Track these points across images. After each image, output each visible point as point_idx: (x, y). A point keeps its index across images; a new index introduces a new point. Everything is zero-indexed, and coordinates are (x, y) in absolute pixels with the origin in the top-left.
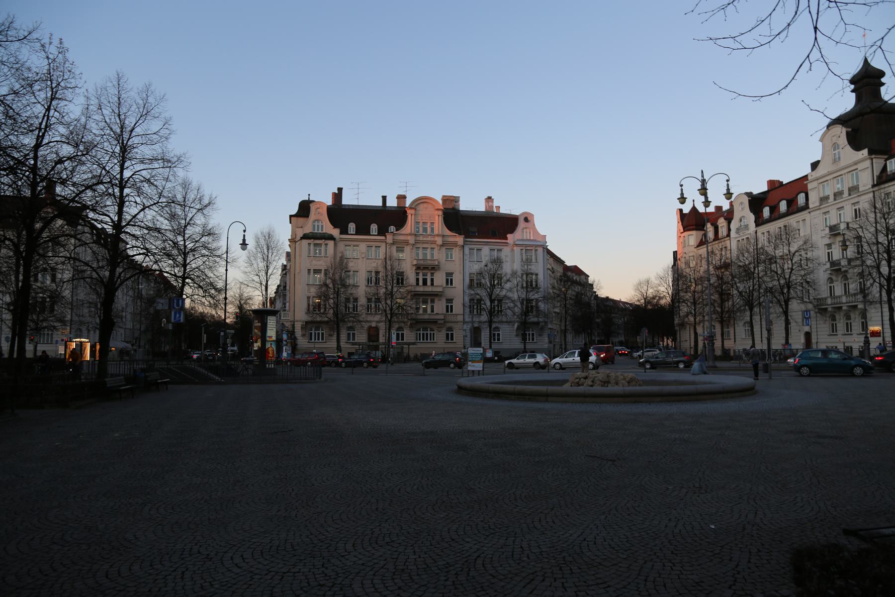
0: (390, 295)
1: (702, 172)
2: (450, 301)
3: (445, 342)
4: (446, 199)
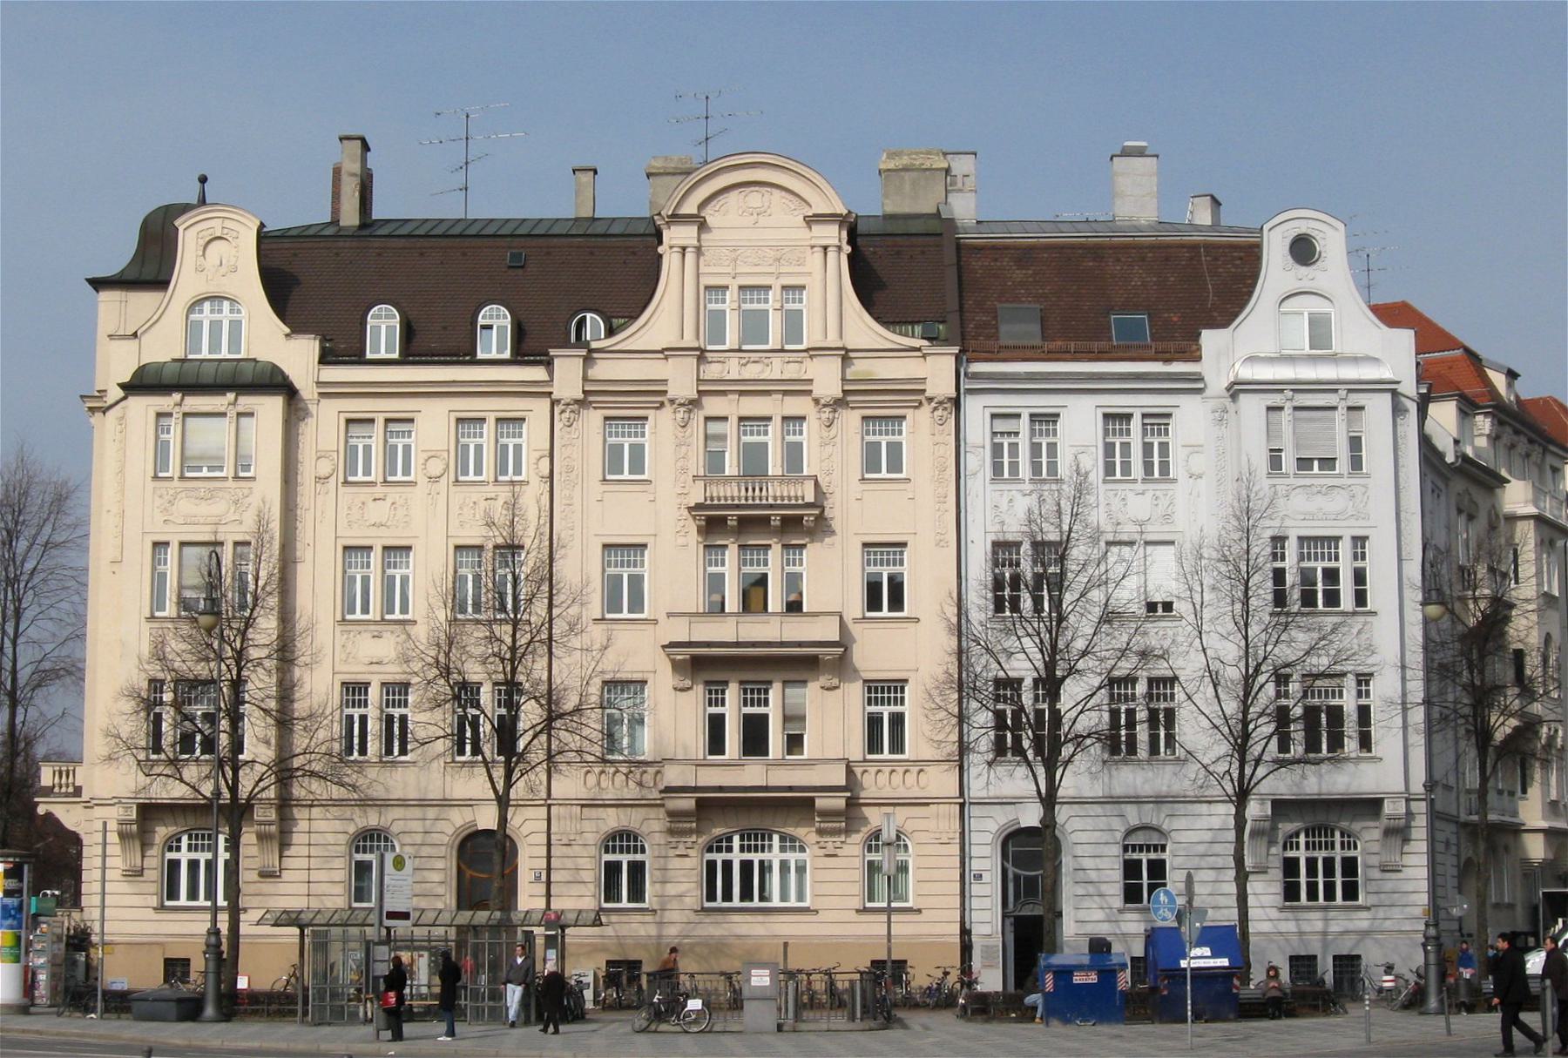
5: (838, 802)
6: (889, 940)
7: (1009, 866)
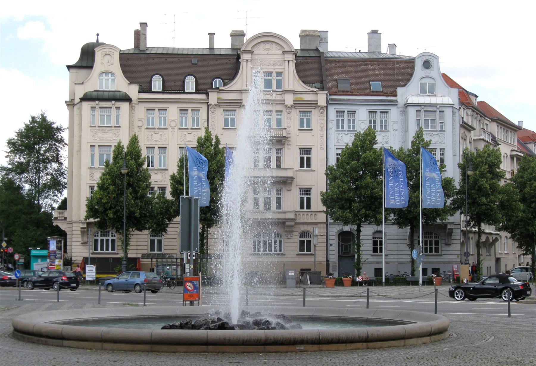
2: (306, 191)
4: (305, 36)
5: (292, 223)
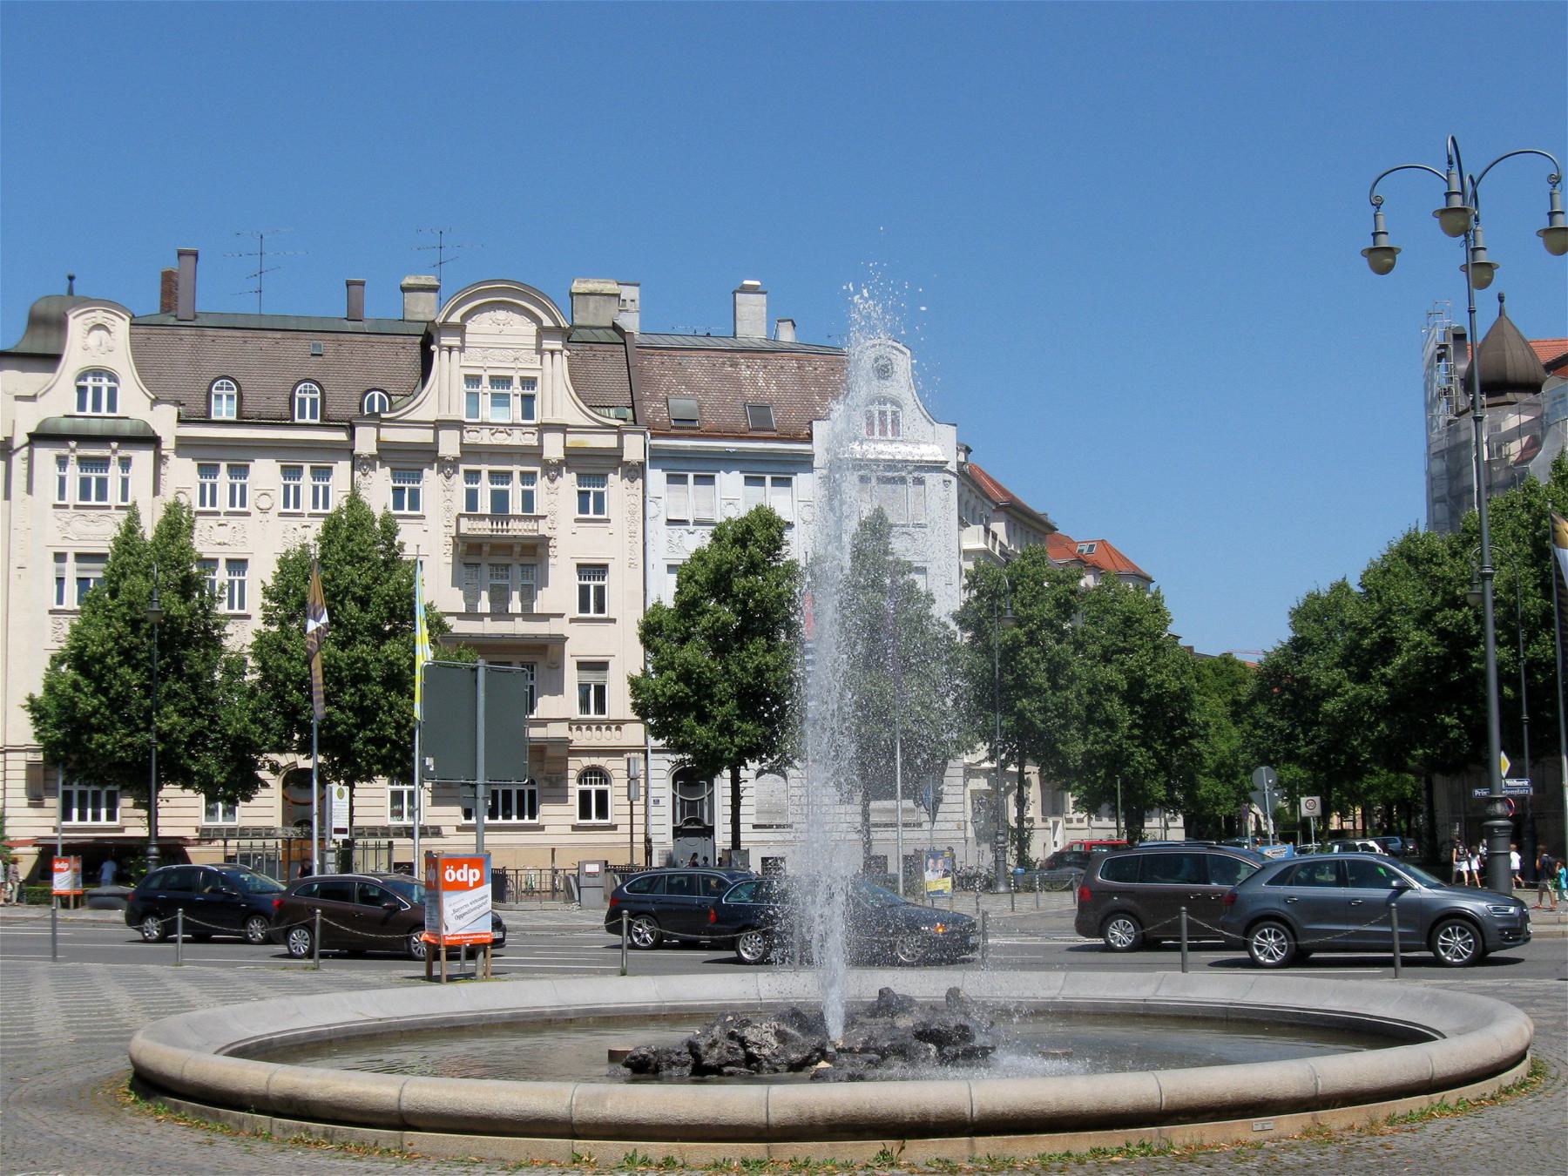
0: (840, 708)
1: (17, 398)
3: (575, 828)
6: (632, 847)
7: (677, 794)
